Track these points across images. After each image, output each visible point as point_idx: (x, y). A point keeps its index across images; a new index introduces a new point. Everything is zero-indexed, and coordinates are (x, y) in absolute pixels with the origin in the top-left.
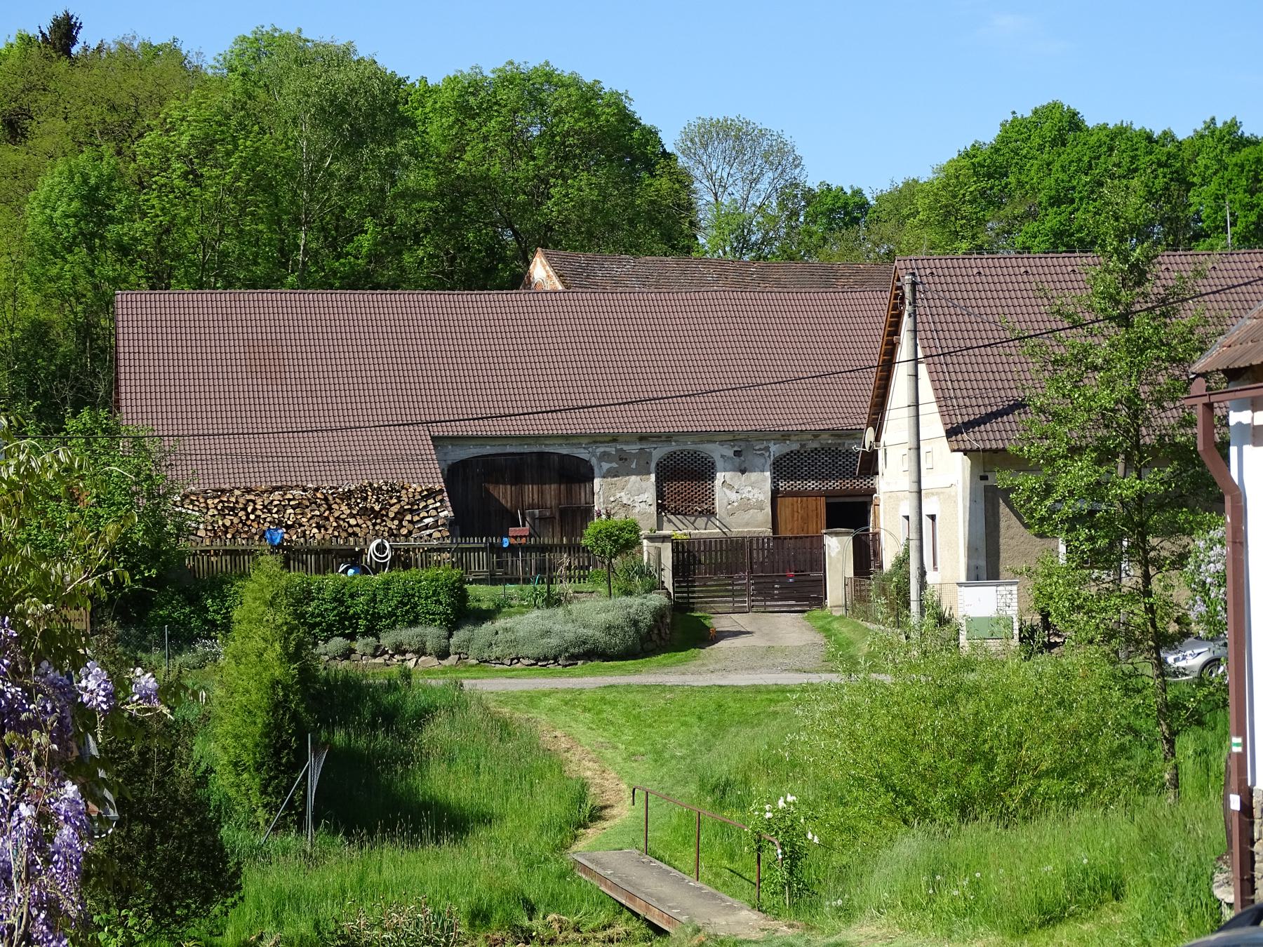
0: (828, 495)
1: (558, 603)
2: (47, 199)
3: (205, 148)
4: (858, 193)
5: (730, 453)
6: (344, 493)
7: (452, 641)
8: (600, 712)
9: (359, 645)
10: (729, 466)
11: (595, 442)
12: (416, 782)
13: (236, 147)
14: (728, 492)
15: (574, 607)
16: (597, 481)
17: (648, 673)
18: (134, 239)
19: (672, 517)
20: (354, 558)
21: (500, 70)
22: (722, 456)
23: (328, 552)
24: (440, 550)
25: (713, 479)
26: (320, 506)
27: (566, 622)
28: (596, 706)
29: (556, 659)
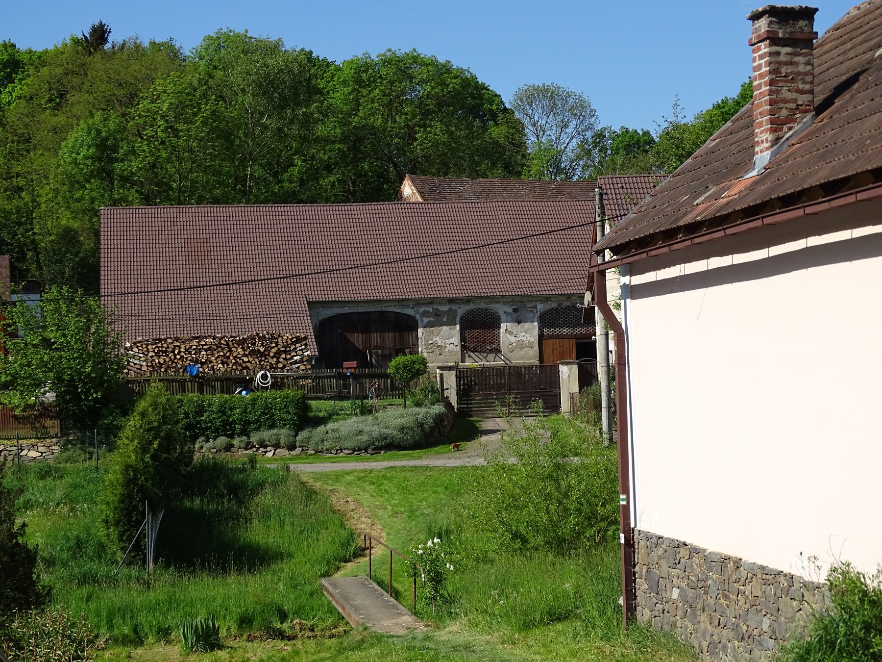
0: (577, 337)
1: (370, 412)
2: (73, 147)
3: (179, 110)
4: (646, 133)
5: (510, 310)
6: (240, 340)
7: (298, 438)
8: (382, 484)
9: (236, 442)
10: (509, 319)
11: (419, 304)
12: (241, 532)
13: (200, 109)
14: (509, 336)
15: (380, 415)
16: (420, 331)
17: (426, 458)
18: (133, 173)
19: (471, 354)
20: (247, 384)
21: (382, 55)
22: (505, 312)
23: (229, 379)
24: (304, 378)
25: (499, 328)
26: (223, 349)
27: (374, 425)
28: (378, 481)
29: (366, 450)
